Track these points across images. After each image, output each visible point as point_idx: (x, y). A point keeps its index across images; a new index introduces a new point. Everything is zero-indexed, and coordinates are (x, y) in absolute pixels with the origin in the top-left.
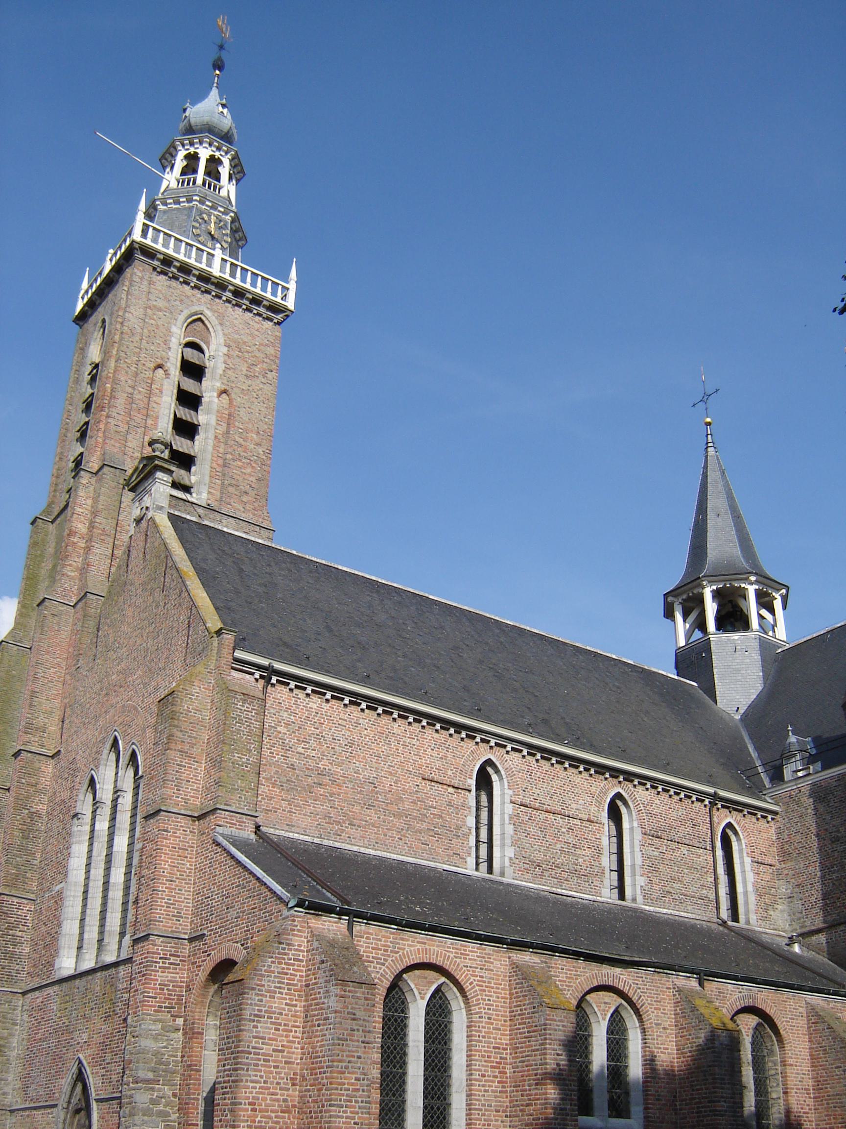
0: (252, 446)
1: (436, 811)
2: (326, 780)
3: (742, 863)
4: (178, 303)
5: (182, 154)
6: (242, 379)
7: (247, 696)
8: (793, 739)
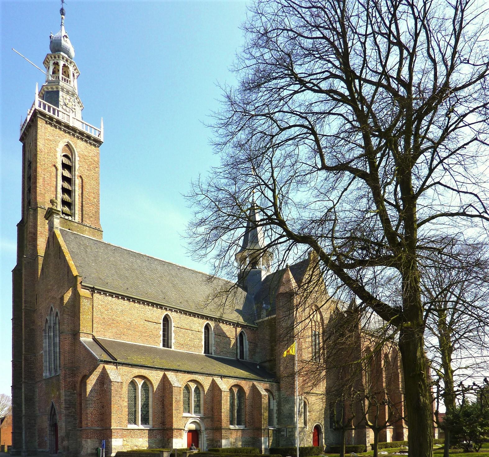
0: (92, 199)
1: (150, 330)
2: (115, 322)
3: (246, 343)
4: (58, 138)
5: (51, 63)
6: (86, 171)
7: (86, 298)
8: (264, 305)
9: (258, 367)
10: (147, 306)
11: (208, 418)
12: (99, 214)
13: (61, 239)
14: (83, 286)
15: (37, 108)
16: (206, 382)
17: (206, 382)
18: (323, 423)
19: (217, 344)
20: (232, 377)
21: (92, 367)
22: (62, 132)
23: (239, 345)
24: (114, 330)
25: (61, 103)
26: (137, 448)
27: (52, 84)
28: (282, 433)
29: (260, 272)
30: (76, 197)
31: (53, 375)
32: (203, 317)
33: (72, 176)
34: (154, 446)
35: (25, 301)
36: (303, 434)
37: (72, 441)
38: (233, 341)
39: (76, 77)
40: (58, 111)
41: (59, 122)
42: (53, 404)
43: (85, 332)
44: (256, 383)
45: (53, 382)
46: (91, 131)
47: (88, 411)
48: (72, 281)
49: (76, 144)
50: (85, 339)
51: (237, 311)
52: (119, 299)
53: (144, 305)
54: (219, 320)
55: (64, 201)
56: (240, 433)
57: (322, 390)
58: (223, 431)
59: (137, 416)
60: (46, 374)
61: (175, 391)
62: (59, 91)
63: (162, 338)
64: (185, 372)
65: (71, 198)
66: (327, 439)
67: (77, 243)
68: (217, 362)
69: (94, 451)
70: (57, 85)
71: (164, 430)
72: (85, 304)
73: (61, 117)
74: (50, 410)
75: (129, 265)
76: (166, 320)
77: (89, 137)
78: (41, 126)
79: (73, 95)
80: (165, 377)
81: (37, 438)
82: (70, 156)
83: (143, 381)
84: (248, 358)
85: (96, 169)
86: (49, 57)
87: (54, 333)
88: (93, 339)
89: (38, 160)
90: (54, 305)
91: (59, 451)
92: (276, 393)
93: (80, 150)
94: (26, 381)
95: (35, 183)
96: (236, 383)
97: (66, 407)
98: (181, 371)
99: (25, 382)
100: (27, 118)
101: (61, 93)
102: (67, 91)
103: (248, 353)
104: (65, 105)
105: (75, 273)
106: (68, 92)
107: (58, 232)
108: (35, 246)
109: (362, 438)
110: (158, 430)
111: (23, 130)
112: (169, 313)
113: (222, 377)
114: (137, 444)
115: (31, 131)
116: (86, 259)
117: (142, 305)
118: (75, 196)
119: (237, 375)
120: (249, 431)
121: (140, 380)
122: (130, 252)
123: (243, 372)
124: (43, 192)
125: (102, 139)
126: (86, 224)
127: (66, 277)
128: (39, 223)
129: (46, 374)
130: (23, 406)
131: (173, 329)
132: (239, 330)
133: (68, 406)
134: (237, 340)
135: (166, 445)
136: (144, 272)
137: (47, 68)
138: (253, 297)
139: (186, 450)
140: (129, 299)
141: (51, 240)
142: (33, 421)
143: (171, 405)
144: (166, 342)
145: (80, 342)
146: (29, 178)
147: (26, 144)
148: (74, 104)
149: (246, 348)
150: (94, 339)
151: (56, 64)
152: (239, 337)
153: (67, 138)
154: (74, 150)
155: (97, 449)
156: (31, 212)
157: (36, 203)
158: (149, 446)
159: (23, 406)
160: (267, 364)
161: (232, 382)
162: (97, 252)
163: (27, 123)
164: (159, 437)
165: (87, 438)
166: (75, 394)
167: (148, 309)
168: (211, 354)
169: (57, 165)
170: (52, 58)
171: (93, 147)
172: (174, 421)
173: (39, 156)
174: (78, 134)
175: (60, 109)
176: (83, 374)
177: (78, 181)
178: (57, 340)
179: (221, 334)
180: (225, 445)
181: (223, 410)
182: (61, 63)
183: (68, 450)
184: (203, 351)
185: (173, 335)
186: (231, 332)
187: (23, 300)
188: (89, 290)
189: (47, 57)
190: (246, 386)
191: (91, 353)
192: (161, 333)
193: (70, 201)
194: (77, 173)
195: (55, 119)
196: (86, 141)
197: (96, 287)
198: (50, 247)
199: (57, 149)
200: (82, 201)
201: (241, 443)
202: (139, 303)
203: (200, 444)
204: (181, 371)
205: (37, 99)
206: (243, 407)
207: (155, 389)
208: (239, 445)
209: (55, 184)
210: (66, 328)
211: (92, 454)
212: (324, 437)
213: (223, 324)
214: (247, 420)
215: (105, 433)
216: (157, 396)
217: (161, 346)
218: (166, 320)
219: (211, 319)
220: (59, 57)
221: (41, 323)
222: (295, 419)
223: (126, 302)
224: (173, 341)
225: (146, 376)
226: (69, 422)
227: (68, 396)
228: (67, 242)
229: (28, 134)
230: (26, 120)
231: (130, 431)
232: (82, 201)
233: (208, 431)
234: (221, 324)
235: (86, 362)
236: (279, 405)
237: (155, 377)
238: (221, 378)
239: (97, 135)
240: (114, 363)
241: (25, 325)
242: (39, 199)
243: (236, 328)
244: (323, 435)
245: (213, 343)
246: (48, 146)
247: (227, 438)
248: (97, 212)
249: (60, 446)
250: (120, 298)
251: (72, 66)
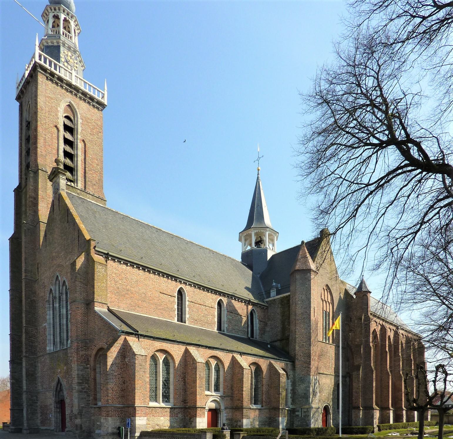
0: (95, 165)
1: (165, 303)
3: (256, 321)
4: (59, 96)
6: (89, 135)
8: (274, 284)
9: (269, 346)
10: (162, 278)
11: (228, 396)
12: (102, 182)
13: (68, 202)
14: (97, 251)
15: (37, 60)
16: (226, 358)
17: (226, 358)
18: (331, 404)
19: (229, 321)
20: (251, 354)
21: (111, 338)
22: (64, 91)
23: (249, 323)
24: (129, 301)
25: (63, 59)
26: (159, 427)
27: (52, 38)
28: (297, 413)
29: (265, 251)
30: (79, 162)
31: (59, 349)
32: (216, 292)
33: (75, 140)
34: (175, 425)
35: (26, 270)
36: (317, 414)
37: (85, 419)
38: (244, 319)
39: (77, 34)
40: (60, 67)
41: (60, 79)
42: (59, 380)
43: (99, 301)
44: (273, 362)
45: (61, 356)
46: (94, 93)
47: (109, 387)
48: (85, 245)
49: (78, 105)
50: (98, 308)
51: (247, 288)
52: (133, 267)
53: (159, 276)
54: (231, 296)
55: (67, 165)
56: (257, 412)
57: (331, 371)
58: (244, 410)
59: (158, 393)
60: (50, 348)
61: (198, 365)
62: (59, 46)
63: (176, 312)
64: (206, 347)
65: (73, 163)
66: (334, 419)
67: (85, 208)
68: (231, 339)
69: (115, 431)
70: (58, 39)
71: (185, 408)
72: (99, 270)
73: (62, 74)
74: (55, 386)
75: (139, 235)
76: (180, 293)
77: (92, 99)
78: (42, 82)
79: (75, 52)
80: (187, 351)
81: (39, 415)
82: (72, 118)
83: (165, 356)
84: (258, 337)
85: (100, 134)
86: (49, 8)
87: (60, 303)
88: (108, 309)
89: (38, 119)
90: (60, 274)
91: (67, 430)
92: (291, 373)
93: (82, 112)
94: (27, 355)
95: (36, 143)
96: (254, 361)
97: (78, 383)
98: (202, 346)
99: (25, 356)
100: (25, 73)
101: (62, 49)
102: (68, 47)
103: (258, 331)
104: (67, 62)
105: (87, 237)
106: (69, 48)
107: (64, 194)
108: (36, 212)
109: (369, 419)
110: (179, 408)
111: (20, 88)
112: (183, 286)
113: (241, 354)
114: (158, 423)
115: (30, 88)
116: (96, 224)
117: (157, 276)
118: (77, 161)
119: (254, 353)
120: (266, 410)
121: (162, 354)
122: (139, 222)
123: (258, 350)
124: (44, 153)
125: (105, 101)
126: (89, 192)
127: (76, 242)
128: (40, 187)
129: (50, 348)
130: (24, 382)
131: (187, 303)
132: (250, 307)
133: (81, 381)
134: (248, 318)
135: (187, 424)
136: (155, 243)
137: (46, 21)
138: (259, 276)
139: (206, 429)
140: (144, 268)
141: (56, 202)
142: (35, 398)
143: (195, 381)
144: (181, 318)
145: (95, 312)
146: (28, 140)
147: (24, 104)
148: (76, 61)
149: (256, 327)
150: (109, 310)
151: (57, 17)
152: (250, 315)
153: (69, 98)
154: (76, 112)
155: (119, 428)
156: (32, 175)
157: (37, 166)
158: (171, 425)
159: (24, 382)
160: (278, 344)
161: (251, 359)
162: (106, 218)
163: (24, 80)
164: (180, 416)
165: (108, 416)
166: (88, 368)
167: (163, 280)
168: (224, 331)
169: (58, 126)
170: (51, 10)
171: (96, 110)
172: (198, 399)
173: (40, 114)
174: (80, 95)
175: (61, 65)
176: (98, 347)
177: (80, 145)
178: (64, 311)
179: (233, 311)
180: (246, 425)
181: (244, 389)
182: (62, 16)
183: (81, 428)
184: (216, 328)
185: (187, 309)
186: (242, 309)
187: (23, 269)
188: (102, 256)
189: (46, 9)
190: (264, 364)
191: (110, 324)
192: (176, 307)
193: (72, 166)
194: (79, 137)
195: (57, 75)
196: (89, 103)
197: (110, 253)
198: (55, 211)
199: (59, 109)
200: (85, 167)
201: (258, 423)
202: (154, 273)
203: (219, 424)
204: (202, 346)
205: (38, 51)
206: (259, 386)
207: (177, 365)
208: (257, 425)
209: (57, 146)
210: (79, 296)
211: (113, 434)
212: (331, 418)
213: (236, 300)
214: (264, 400)
215: (128, 411)
216: (179, 373)
217: (175, 320)
218: (180, 293)
219: (224, 294)
220: (59, 10)
221: (43, 293)
222: (311, 399)
223: (141, 272)
224: (187, 316)
225: (168, 350)
226: (82, 399)
227: (81, 371)
228: (75, 205)
229: (26, 92)
230: (24, 76)
231: (151, 409)
232: (85, 167)
233: (228, 410)
234: (233, 301)
235: (102, 334)
236: (294, 384)
237: (177, 352)
238: (241, 355)
239: (101, 96)
240: (136, 334)
241: (25, 295)
242: (40, 161)
243: (247, 306)
244: (331, 416)
245: (226, 320)
246: (49, 104)
247: (248, 418)
248: (101, 180)
249: (68, 424)
250: (135, 267)
251: (74, 20)
